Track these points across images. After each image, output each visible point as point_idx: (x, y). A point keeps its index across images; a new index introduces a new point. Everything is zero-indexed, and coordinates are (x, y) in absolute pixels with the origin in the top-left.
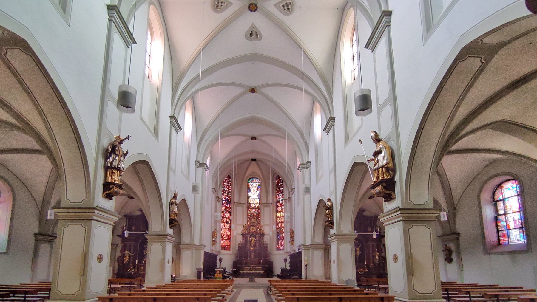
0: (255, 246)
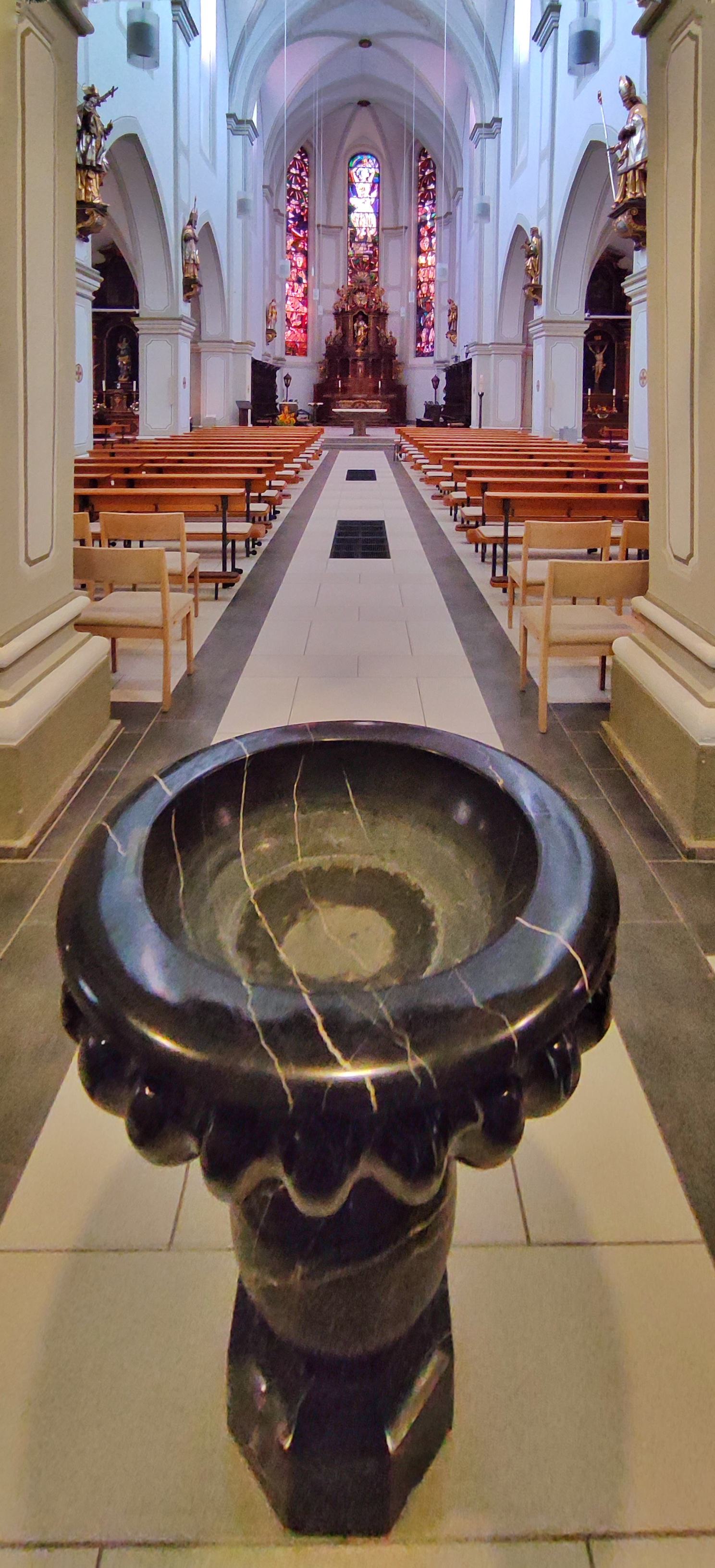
0: (366, 342)
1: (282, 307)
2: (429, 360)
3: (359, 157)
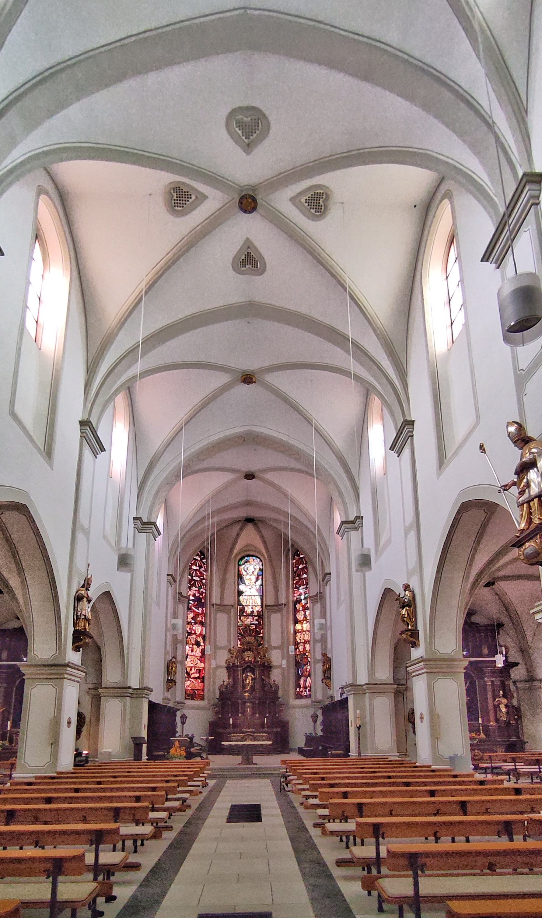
0: (253, 688)
1: (182, 663)
2: (307, 702)
3: (246, 558)
